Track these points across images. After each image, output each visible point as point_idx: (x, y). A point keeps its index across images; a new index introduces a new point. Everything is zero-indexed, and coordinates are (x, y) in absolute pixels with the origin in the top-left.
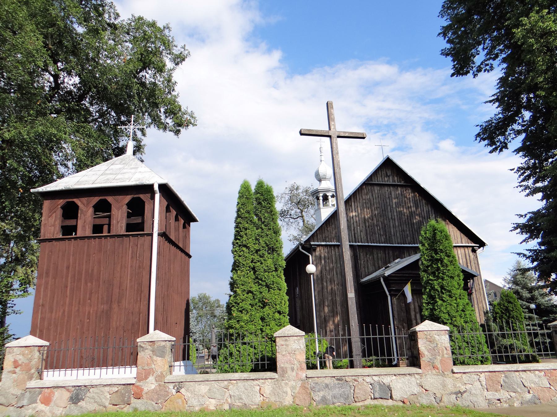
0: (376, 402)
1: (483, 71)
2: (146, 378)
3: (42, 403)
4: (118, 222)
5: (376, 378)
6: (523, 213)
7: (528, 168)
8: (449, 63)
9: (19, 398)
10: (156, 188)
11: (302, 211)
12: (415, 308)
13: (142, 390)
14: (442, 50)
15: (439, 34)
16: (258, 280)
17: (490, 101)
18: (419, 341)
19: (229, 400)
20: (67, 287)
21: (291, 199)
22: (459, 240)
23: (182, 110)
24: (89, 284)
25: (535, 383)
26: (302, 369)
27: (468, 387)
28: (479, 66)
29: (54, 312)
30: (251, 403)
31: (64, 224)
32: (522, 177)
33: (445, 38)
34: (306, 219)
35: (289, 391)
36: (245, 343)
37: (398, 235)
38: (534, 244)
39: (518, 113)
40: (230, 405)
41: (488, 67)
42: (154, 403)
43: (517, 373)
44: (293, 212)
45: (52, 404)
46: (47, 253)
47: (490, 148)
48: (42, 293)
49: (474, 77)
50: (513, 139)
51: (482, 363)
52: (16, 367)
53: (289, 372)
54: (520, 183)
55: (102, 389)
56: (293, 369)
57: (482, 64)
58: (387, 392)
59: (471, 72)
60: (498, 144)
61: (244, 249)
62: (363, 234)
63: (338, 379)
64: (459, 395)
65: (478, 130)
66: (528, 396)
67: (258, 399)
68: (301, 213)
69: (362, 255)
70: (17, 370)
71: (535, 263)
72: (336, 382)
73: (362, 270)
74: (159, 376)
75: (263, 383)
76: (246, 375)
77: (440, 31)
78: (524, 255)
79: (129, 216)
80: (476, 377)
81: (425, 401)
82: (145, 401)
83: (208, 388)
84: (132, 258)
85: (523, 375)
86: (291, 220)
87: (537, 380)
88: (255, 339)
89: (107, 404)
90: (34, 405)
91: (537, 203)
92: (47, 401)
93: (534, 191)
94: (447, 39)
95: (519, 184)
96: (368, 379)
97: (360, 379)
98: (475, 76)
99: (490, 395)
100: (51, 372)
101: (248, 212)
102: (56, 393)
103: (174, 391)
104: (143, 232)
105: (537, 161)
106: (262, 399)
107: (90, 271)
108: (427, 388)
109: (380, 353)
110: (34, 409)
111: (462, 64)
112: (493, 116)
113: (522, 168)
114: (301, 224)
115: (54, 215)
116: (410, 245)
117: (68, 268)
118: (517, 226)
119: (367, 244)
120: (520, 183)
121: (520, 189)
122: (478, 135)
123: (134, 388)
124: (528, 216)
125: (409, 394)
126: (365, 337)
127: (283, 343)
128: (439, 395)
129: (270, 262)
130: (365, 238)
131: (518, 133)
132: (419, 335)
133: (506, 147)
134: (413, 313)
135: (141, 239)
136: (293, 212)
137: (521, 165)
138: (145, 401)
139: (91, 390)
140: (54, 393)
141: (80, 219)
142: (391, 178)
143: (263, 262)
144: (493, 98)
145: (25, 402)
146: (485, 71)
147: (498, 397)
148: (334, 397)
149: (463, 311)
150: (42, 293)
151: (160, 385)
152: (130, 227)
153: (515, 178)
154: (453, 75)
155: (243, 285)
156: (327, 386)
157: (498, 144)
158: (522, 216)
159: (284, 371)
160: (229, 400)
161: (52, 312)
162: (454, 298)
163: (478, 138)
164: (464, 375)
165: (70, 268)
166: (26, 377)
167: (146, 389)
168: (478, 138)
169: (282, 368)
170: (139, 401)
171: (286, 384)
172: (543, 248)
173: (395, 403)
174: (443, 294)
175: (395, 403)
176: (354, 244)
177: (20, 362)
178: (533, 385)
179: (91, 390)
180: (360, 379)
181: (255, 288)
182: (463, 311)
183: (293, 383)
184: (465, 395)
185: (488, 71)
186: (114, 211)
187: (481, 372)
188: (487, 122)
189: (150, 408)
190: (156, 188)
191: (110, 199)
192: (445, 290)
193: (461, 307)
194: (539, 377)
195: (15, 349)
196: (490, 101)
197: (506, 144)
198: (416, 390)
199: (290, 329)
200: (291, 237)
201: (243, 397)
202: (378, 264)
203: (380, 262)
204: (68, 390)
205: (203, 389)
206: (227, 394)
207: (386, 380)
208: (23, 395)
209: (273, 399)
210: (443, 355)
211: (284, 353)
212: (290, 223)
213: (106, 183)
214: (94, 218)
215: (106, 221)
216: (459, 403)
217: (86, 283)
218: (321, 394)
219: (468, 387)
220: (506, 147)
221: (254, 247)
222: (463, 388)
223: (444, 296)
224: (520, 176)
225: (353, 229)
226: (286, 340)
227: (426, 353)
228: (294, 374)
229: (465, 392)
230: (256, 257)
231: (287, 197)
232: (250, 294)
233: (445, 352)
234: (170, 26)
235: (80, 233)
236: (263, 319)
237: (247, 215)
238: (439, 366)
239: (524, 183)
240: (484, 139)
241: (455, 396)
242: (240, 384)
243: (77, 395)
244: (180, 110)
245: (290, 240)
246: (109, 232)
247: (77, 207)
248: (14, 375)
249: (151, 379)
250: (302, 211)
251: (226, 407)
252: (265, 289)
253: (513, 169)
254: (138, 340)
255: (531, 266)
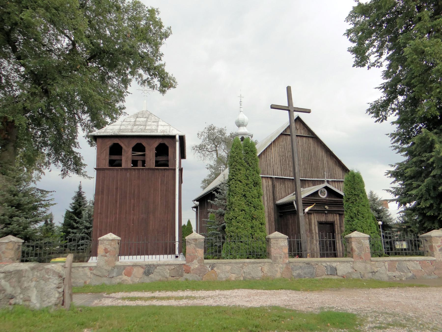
0: (328, 277)
1: (376, 66)
2: (192, 261)
3: (125, 275)
4: (150, 160)
5: (328, 264)
6: (394, 164)
7: (398, 135)
8: (352, 58)
9: (109, 272)
10: (177, 137)
11: (216, 146)
12: (315, 222)
13: (190, 268)
14: (349, 48)
15: (344, 34)
16: (249, 204)
17: (379, 88)
18: (353, 243)
19: (243, 275)
20: (117, 202)
21: (209, 137)
22: (342, 177)
23: (169, 76)
24: (132, 201)
25: (414, 267)
26: (286, 258)
27: (379, 269)
28: (373, 63)
29: (109, 218)
30: (256, 276)
31: (111, 159)
32: (394, 140)
33: (348, 37)
34: (219, 152)
35: (278, 269)
36: (241, 242)
37: (302, 171)
38: (398, 185)
39: (396, 97)
40: (244, 277)
41: (379, 64)
42: (197, 276)
43: (405, 262)
44: (209, 147)
45: (132, 276)
46: (101, 178)
47: (376, 119)
48: (99, 205)
49: (368, 69)
50: (391, 114)
51: (380, 256)
52: (106, 253)
53: (279, 259)
54: (392, 144)
55: (165, 267)
56: (281, 257)
57: (375, 62)
58: (334, 271)
59: (367, 65)
60: (381, 117)
61: (239, 182)
62: (279, 170)
63: (307, 264)
64: (374, 273)
65: (368, 107)
66: (410, 275)
67: (260, 274)
68: (216, 148)
69: (277, 184)
70: (107, 254)
71: (397, 197)
72: (306, 265)
73: (277, 195)
74: (200, 260)
75: (263, 265)
76: (253, 260)
77: (346, 32)
78: (391, 191)
79: (157, 155)
80: (383, 264)
81: (355, 276)
82: (192, 274)
83: (230, 267)
84: (161, 184)
85: (408, 263)
86: (207, 153)
87: (415, 266)
88: (247, 239)
89: (168, 276)
90: (120, 276)
91: (402, 158)
92: (129, 274)
93: (402, 150)
94: (349, 38)
95: (392, 145)
96: (324, 264)
97: (320, 264)
98: (369, 68)
99: (390, 274)
100: (123, 257)
101: (241, 159)
102: (135, 269)
103: (210, 269)
104: (167, 168)
105: (405, 131)
106: (262, 274)
107: (133, 192)
108: (356, 269)
109: (329, 250)
110: (121, 279)
111: (361, 59)
112: (380, 98)
113: (393, 134)
114: (215, 156)
115: (105, 152)
116: (310, 179)
117: (117, 189)
118: (390, 172)
119: (281, 177)
120: (392, 144)
121: (393, 148)
122: (369, 110)
123: (185, 267)
124: (396, 166)
125: (346, 272)
126: (331, 240)
127: (275, 242)
128: (362, 274)
129: (255, 192)
130: (280, 172)
131: (394, 110)
132: (353, 240)
133: (386, 119)
134: (313, 226)
135: (167, 173)
136: (209, 147)
137: (394, 132)
138: (192, 274)
139: (158, 267)
140: (133, 269)
141: (124, 156)
142: (299, 131)
143: (251, 191)
144: (381, 86)
145: (114, 274)
146: (377, 67)
147: (394, 275)
148: (305, 274)
149: (370, 226)
150: (99, 205)
151: (201, 265)
152: (158, 164)
153: (389, 141)
154: (354, 66)
155: (238, 206)
156: (301, 267)
157: (381, 117)
158: (392, 166)
159: (276, 258)
160: (243, 275)
161: (107, 219)
162: (365, 218)
163: (368, 112)
164: (377, 263)
165: (119, 189)
166: (114, 259)
167: (192, 267)
168: (368, 112)
169: (275, 256)
170: (188, 275)
171: (277, 266)
172: (403, 186)
173: (339, 277)
174: (358, 215)
175: (339, 277)
176: (273, 176)
177: (109, 250)
178: (413, 269)
179: (158, 267)
180: (320, 264)
181: (246, 208)
182: (370, 226)
183: (281, 266)
184: (376, 273)
185: (379, 67)
186: (147, 152)
187: (386, 261)
188: (375, 102)
189: (196, 279)
190: (177, 137)
191: (144, 143)
192: (360, 213)
193: (369, 224)
194: (417, 264)
195: (105, 242)
196: (379, 88)
197: (386, 118)
198: (350, 270)
199: (277, 234)
200: (209, 166)
201: (252, 273)
202: (288, 191)
203: (289, 190)
204: (142, 267)
205: (228, 268)
206: (242, 271)
207: (334, 265)
208: (112, 270)
209: (269, 274)
210: (366, 251)
211: (275, 248)
212: (206, 155)
213: (139, 132)
214: (133, 155)
215: (141, 158)
216: (374, 278)
217: (130, 200)
218: (297, 272)
219: (379, 269)
220: (386, 119)
221: (244, 181)
222: (376, 270)
223: (359, 217)
224: (392, 139)
225: (272, 166)
226: (277, 240)
227: (356, 250)
228: (282, 260)
229: (377, 272)
230: (246, 188)
231: (206, 135)
232: (243, 212)
233: (367, 249)
234: (159, 10)
235: (124, 166)
236: (252, 227)
237: (240, 161)
238: (363, 257)
239: (395, 144)
240: (372, 113)
241: (371, 274)
242: (250, 266)
243: (149, 270)
244: (167, 76)
245: (208, 168)
246: (143, 165)
247: (121, 148)
248: (105, 258)
249: (195, 261)
250: (216, 146)
251: (242, 279)
252: (252, 209)
253: (388, 134)
254: (186, 238)
255: (394, 198)
